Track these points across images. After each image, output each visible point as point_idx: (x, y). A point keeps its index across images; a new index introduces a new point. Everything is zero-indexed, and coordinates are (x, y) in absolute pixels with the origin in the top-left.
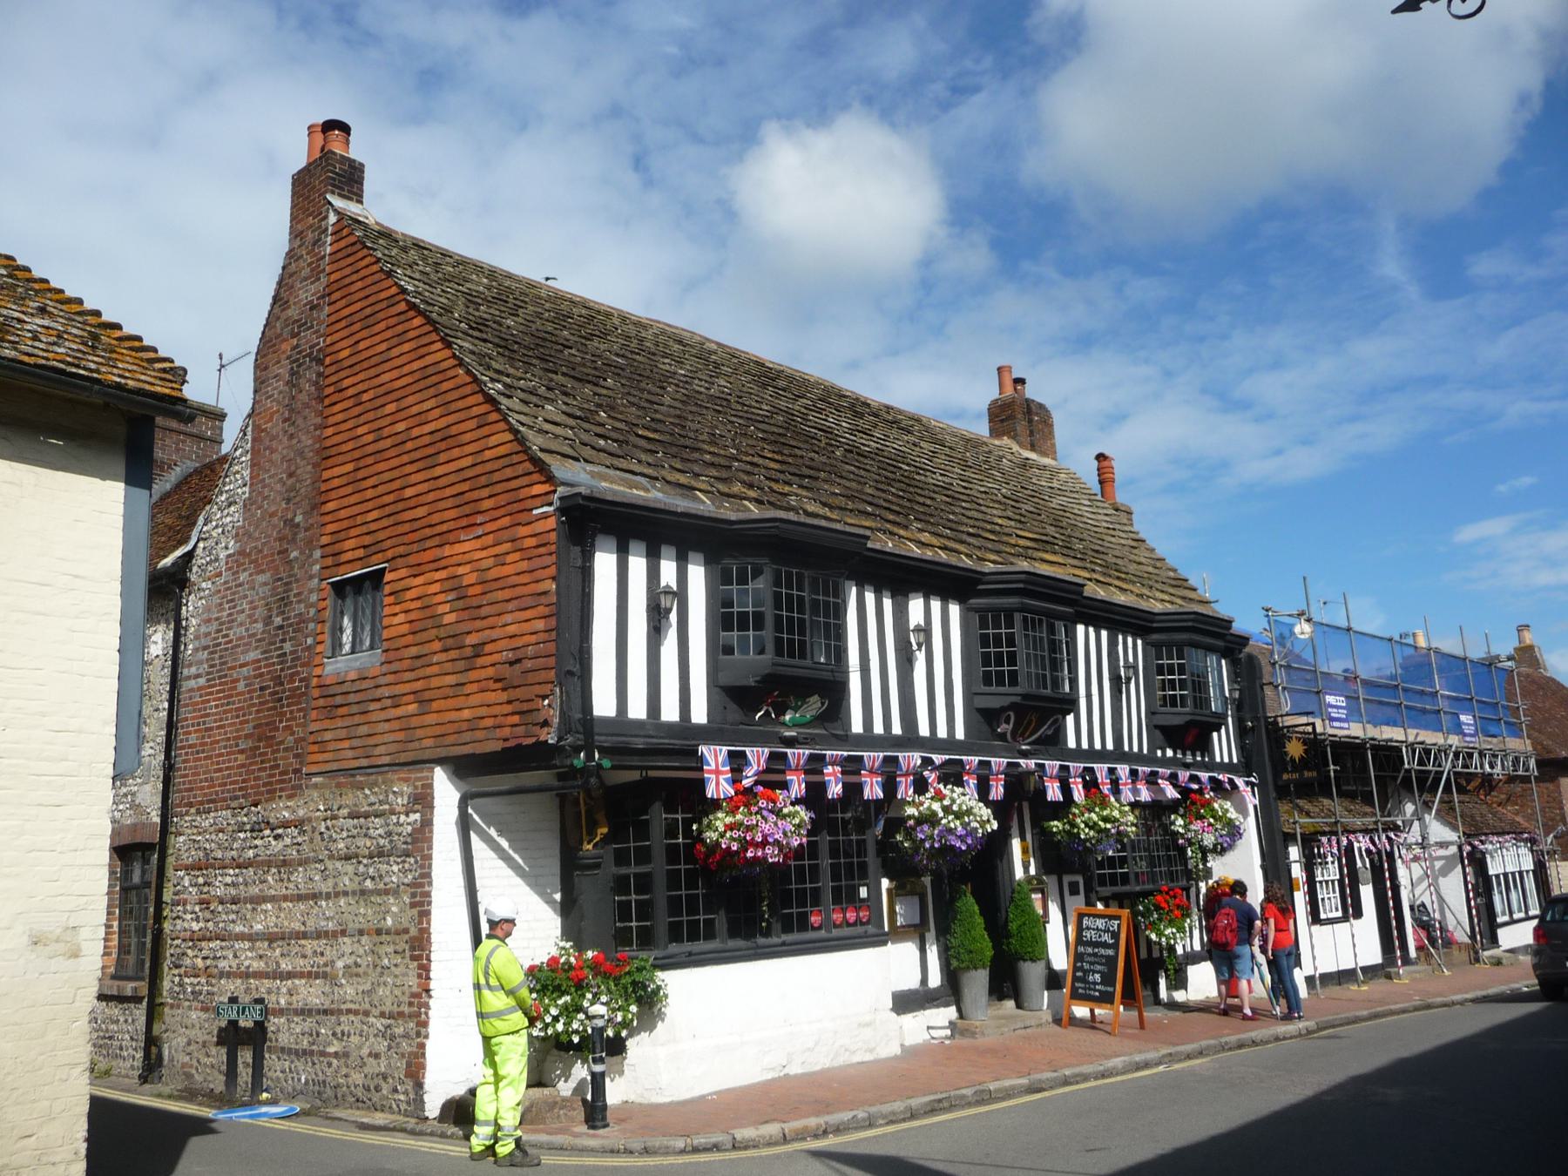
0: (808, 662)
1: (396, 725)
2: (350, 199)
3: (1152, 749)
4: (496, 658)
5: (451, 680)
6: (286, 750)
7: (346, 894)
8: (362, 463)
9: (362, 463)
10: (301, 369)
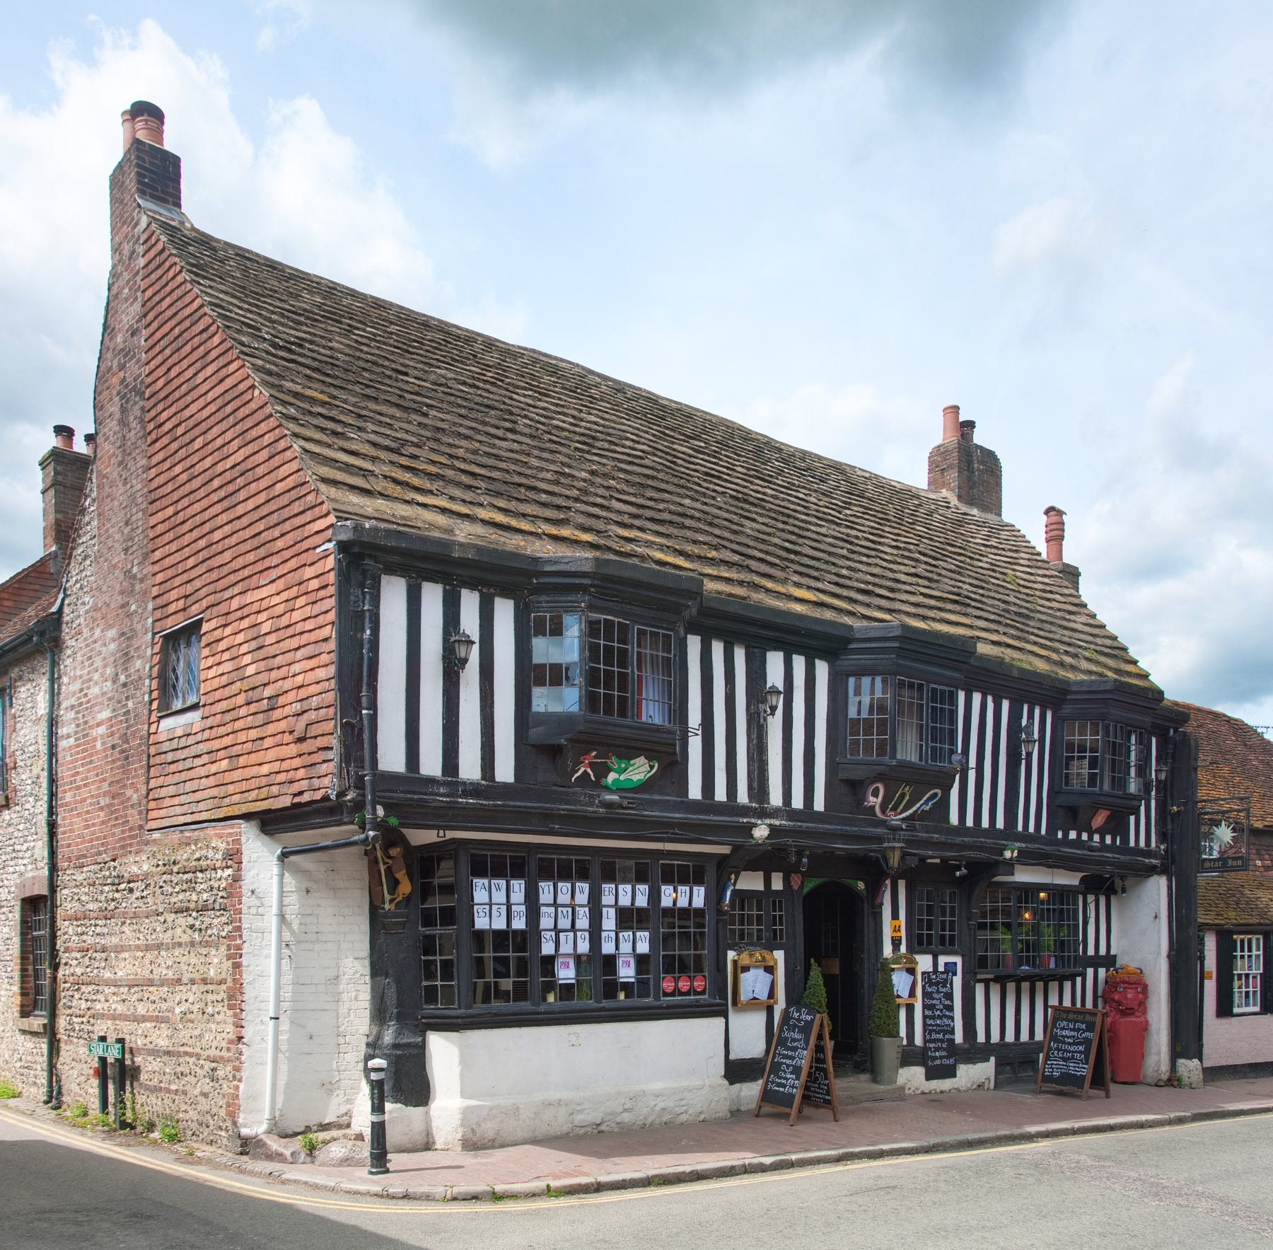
0: (628, 721)
1: (212, 781)
2: (165, 201)
3: (1052, 829)
4: (287, 711)
5: (253, 734)
6: (132, 806)
7: (180, 945)
8: (180, 506)
9: (180, 506)
10: (129, 406)
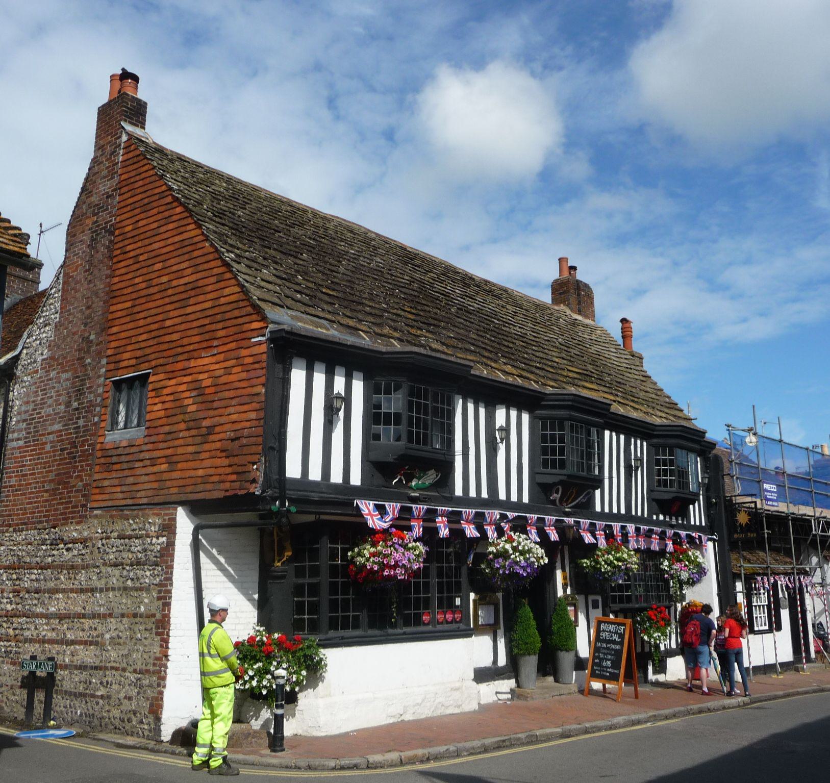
0: (429, 448)
3: (650, 513)
4: (222, 436)
7: (113, 589)
8: (137, 302)
9: (137, 302)
